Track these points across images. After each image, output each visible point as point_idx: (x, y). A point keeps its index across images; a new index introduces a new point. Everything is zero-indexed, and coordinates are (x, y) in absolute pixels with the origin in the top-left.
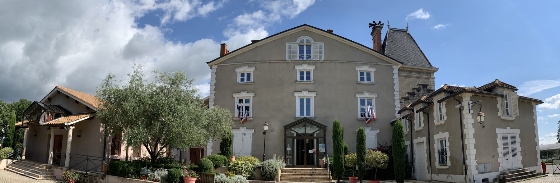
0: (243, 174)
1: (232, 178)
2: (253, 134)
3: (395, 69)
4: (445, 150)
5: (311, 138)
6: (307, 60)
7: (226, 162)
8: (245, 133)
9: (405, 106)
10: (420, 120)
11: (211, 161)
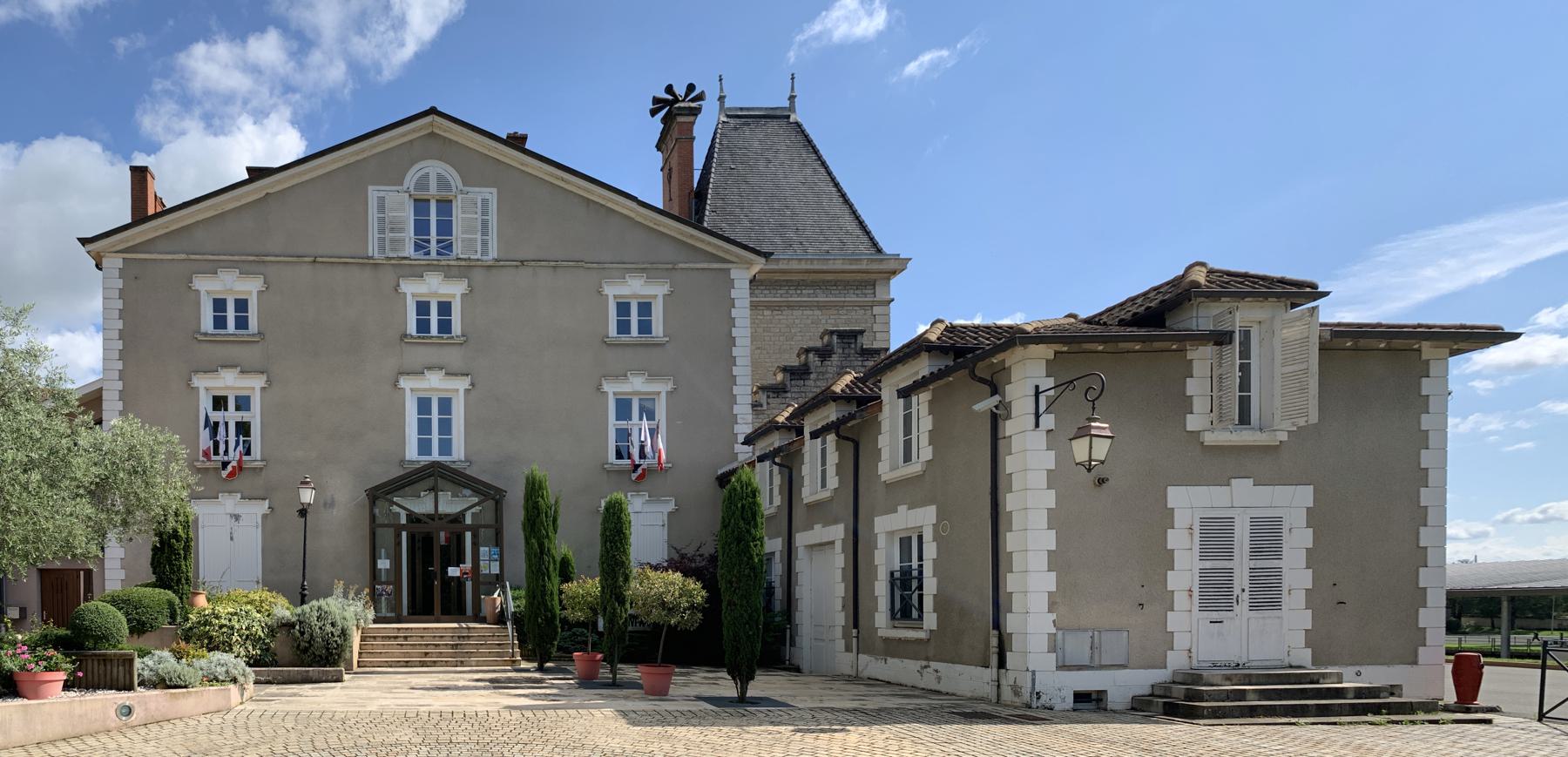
0: (235, 649)
1: (196, 663)
2: (265, 517)
3: (741, 279)
4: (915, 573)
5: (456, 527)
6: (439, 257)
7: (175, 611)
8: (236, 512)
9: (772, 416)
10: (824, 463)
11: (120, 610)
